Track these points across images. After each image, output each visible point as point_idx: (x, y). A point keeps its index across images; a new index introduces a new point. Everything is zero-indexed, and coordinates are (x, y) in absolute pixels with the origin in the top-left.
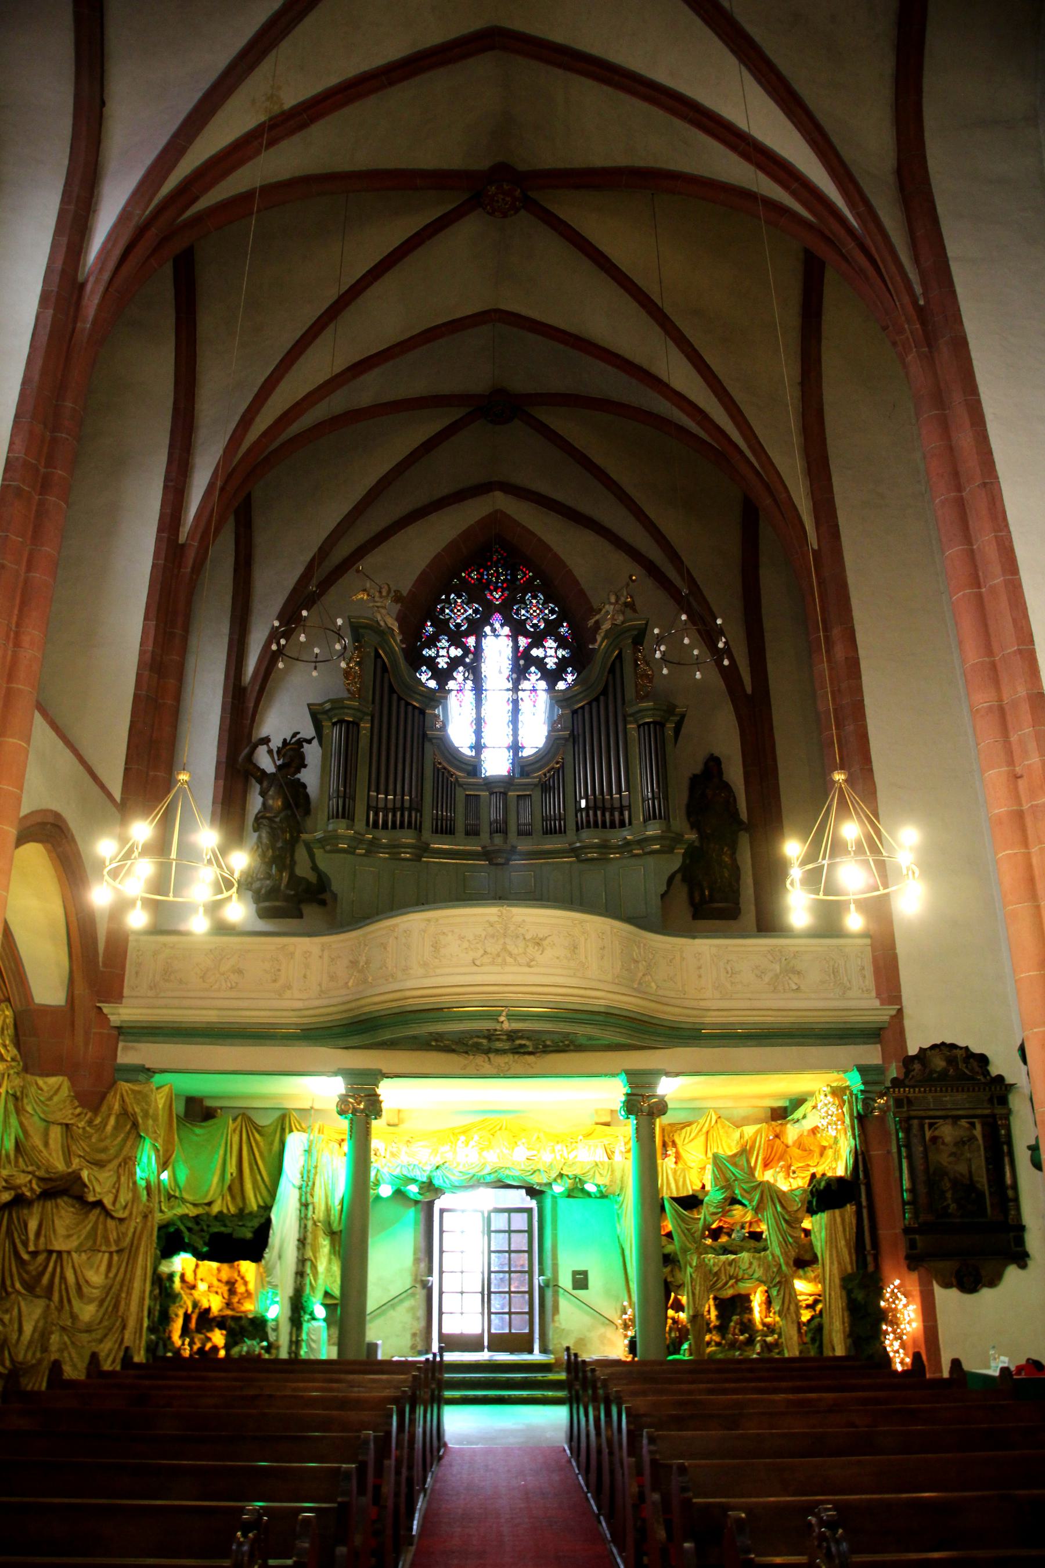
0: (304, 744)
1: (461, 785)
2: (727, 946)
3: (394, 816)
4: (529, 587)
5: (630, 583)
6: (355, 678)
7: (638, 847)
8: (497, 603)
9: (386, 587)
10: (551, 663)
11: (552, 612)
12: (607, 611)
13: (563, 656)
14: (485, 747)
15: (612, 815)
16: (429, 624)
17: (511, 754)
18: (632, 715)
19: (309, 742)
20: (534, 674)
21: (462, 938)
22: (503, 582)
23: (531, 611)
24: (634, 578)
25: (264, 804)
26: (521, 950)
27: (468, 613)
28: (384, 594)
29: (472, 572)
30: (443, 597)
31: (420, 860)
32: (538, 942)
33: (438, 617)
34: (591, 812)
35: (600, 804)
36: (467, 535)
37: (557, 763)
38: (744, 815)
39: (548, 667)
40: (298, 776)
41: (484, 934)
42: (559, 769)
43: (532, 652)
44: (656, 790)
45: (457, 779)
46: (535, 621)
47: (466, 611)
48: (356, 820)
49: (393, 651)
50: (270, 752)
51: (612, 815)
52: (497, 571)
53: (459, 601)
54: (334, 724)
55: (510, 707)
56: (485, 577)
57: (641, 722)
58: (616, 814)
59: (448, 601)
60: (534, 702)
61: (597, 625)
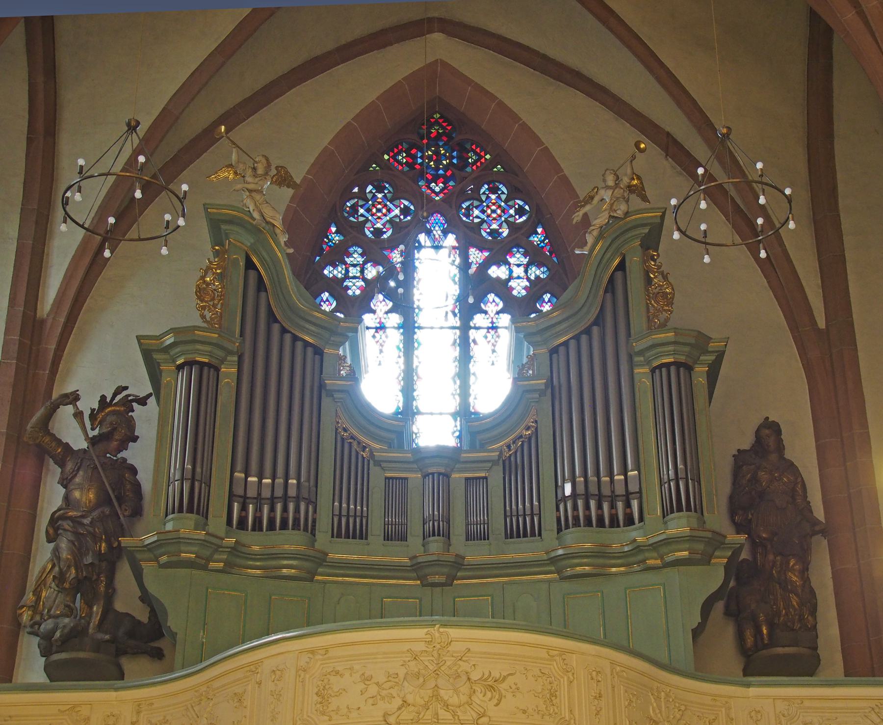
0: (135, 405)
1: (378, 463)
2: (802, 699)
3: (272, 509)
4: (485, 176)
5: (638, 154)
6: (213, 299)
7: (655, 554)
8: (437, 198)
9: (264, 160)
10: (519, 287)
11: (520, 212)
12: (602, 200)
13: (537, 278)
14: (419, 413)
15: (613, 506)
16: (334, 229)
17: (458, 423)
18: (641, 353)
19: (143, 401)
20: (493, 303)
21: (366, 679)
22: (446, 168)
23: (489, 211)
24: (642, 146)
25: (67, 498)
26: (464, 699)
27: (393, 214)
28: (260, 171)
29: (399, 153)
30: (356, 190)
31: (311, 580)
32: (491, 685)
33: (347, 219)
34: (580, 503)
35: (593, 489)
36: (390, 96)
37: (528, 428)
38: (819, 513)
39: (515, 293)
40: (123, 454)
41: (402, 672)
42: (530, 439)
43: (490, 272)
44: (680, 466)
45: (371, 452)
46: (494, 226)
47: (390, 211)
48: (210, 516)
49: (276, 261)
50: (78, 415)
51: (613, 506)
52: (437, 153)
53: (380, 196)
54: (180, 367)
55: (456, 352)
56: (420, 161)
57: (656, 363)
58: (620, 505)
59: (362, 195)
60: (494, 345)
61: (586, 221)
